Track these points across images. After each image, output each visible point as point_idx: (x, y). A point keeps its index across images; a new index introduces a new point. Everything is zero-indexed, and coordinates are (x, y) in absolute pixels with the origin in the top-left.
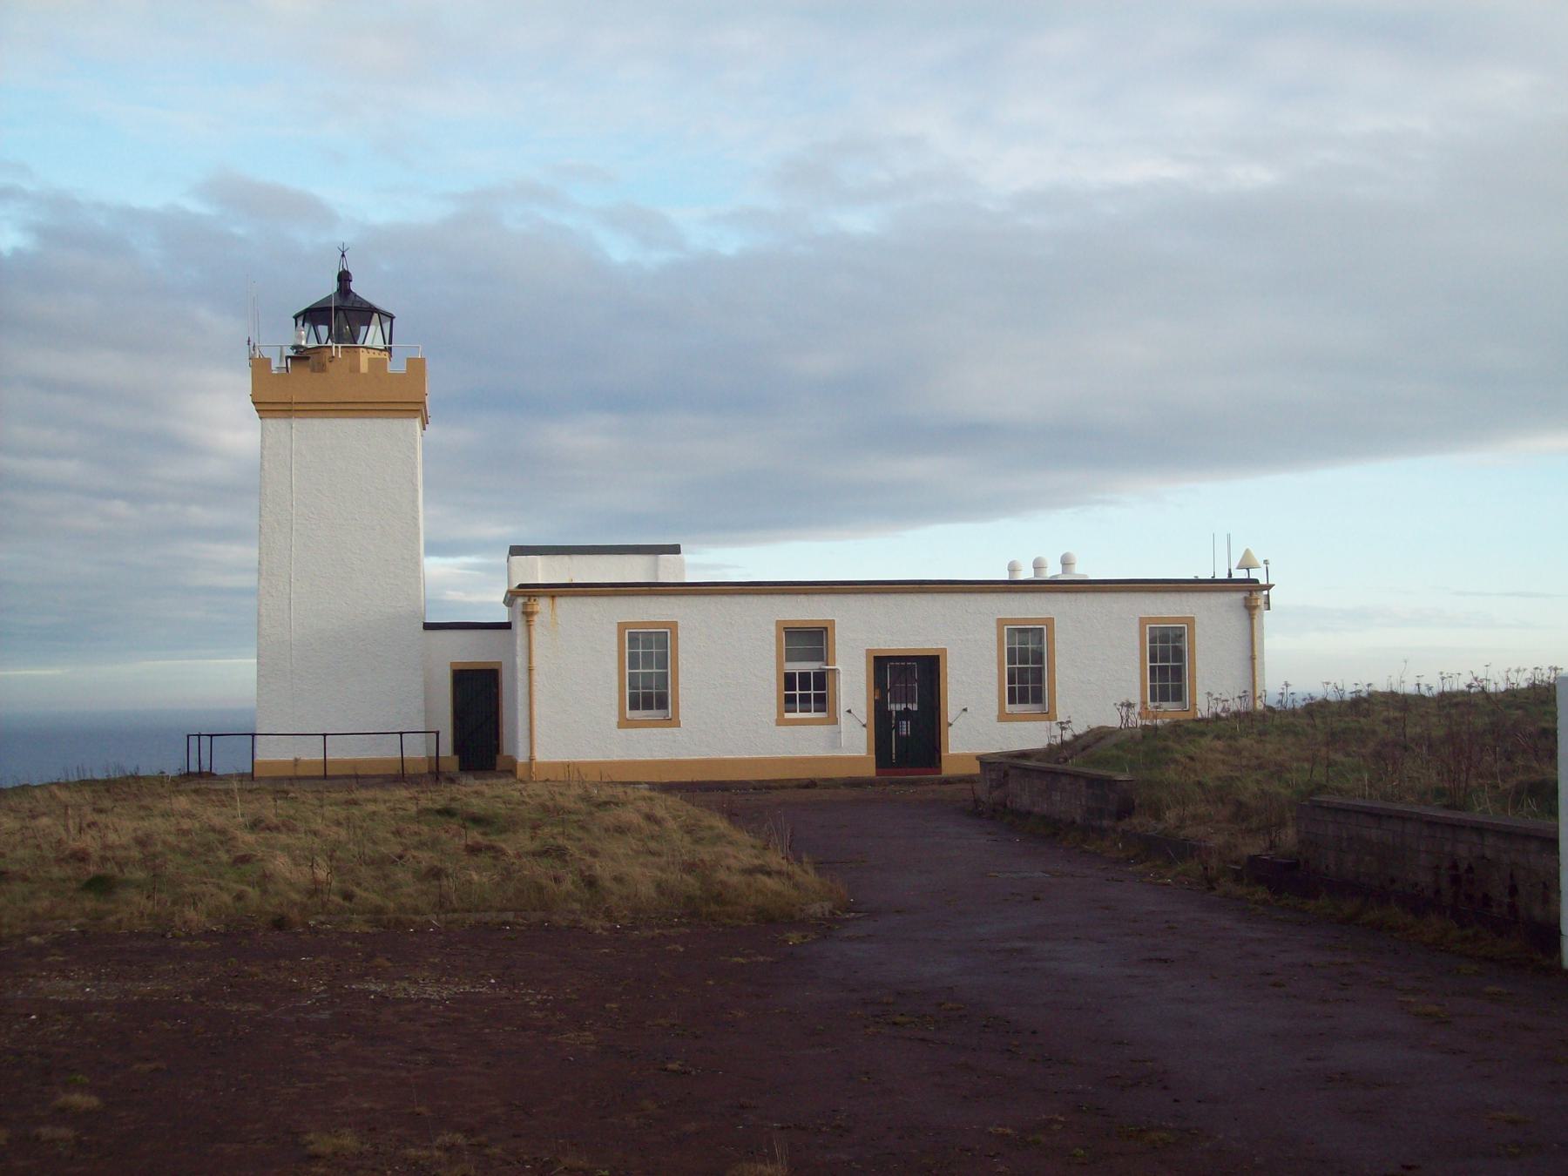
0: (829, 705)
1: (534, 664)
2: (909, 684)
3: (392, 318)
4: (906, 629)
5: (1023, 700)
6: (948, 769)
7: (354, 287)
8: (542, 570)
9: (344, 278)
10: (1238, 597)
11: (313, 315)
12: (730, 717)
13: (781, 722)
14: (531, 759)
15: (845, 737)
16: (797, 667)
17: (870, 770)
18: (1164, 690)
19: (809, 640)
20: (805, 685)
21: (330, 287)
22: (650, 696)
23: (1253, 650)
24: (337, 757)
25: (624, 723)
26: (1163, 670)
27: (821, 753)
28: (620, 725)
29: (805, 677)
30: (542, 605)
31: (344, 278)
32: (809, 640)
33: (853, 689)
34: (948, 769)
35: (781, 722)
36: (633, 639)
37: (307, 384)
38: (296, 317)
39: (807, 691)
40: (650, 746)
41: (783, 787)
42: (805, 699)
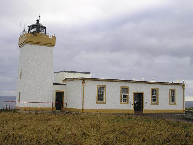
0: (104, 99)
1: (84, 91)
2: (139, 97)
3: (46, 29)
4: (139, 89)
5: (100, 100)
6: (144, 112)
7: (40, 22)
8: (70, 76)
9: (38, 21)
10: (182, 87)
11: (33, 27)
12: (113, 102)
13: (121, 103)
14: (83, 109)
15: (129, 106)
16: (123, 94)
17: (133, 112)
18: (100, 98)
19: (125, 90)
20: (124, 98)
21: (36, 22)
22: (101, 97)
23: (184, 95)
24: (41, 107)
25: (97, 103)
26: (100, 95)
27: (126, 109)
28: (97, 103)
29: (124, 96)
30: (86, 81)
31: (38, 21)
32: (125, 90)
33: (131, 98)
34: (144, 112)
35: (121, 103)
36: (103, 88)
37: (34, 39)
38: (29, 27)
39: (124, 98)
40: (101, 107)
41: (151, 114)
42: (124, 100)
